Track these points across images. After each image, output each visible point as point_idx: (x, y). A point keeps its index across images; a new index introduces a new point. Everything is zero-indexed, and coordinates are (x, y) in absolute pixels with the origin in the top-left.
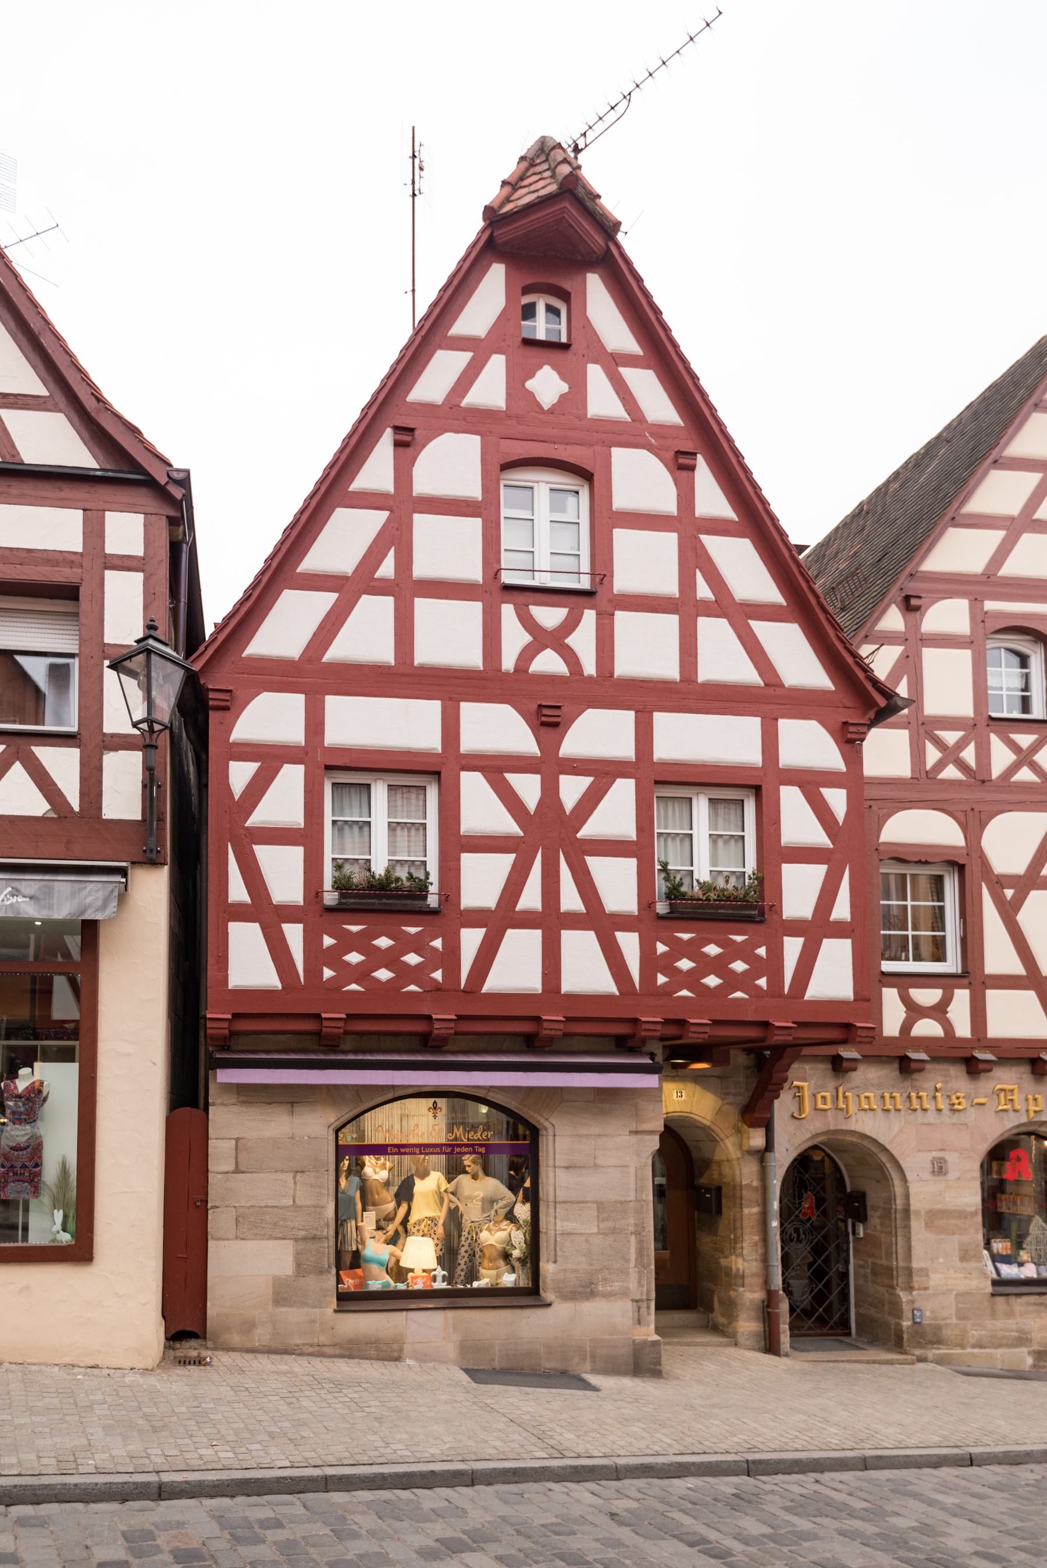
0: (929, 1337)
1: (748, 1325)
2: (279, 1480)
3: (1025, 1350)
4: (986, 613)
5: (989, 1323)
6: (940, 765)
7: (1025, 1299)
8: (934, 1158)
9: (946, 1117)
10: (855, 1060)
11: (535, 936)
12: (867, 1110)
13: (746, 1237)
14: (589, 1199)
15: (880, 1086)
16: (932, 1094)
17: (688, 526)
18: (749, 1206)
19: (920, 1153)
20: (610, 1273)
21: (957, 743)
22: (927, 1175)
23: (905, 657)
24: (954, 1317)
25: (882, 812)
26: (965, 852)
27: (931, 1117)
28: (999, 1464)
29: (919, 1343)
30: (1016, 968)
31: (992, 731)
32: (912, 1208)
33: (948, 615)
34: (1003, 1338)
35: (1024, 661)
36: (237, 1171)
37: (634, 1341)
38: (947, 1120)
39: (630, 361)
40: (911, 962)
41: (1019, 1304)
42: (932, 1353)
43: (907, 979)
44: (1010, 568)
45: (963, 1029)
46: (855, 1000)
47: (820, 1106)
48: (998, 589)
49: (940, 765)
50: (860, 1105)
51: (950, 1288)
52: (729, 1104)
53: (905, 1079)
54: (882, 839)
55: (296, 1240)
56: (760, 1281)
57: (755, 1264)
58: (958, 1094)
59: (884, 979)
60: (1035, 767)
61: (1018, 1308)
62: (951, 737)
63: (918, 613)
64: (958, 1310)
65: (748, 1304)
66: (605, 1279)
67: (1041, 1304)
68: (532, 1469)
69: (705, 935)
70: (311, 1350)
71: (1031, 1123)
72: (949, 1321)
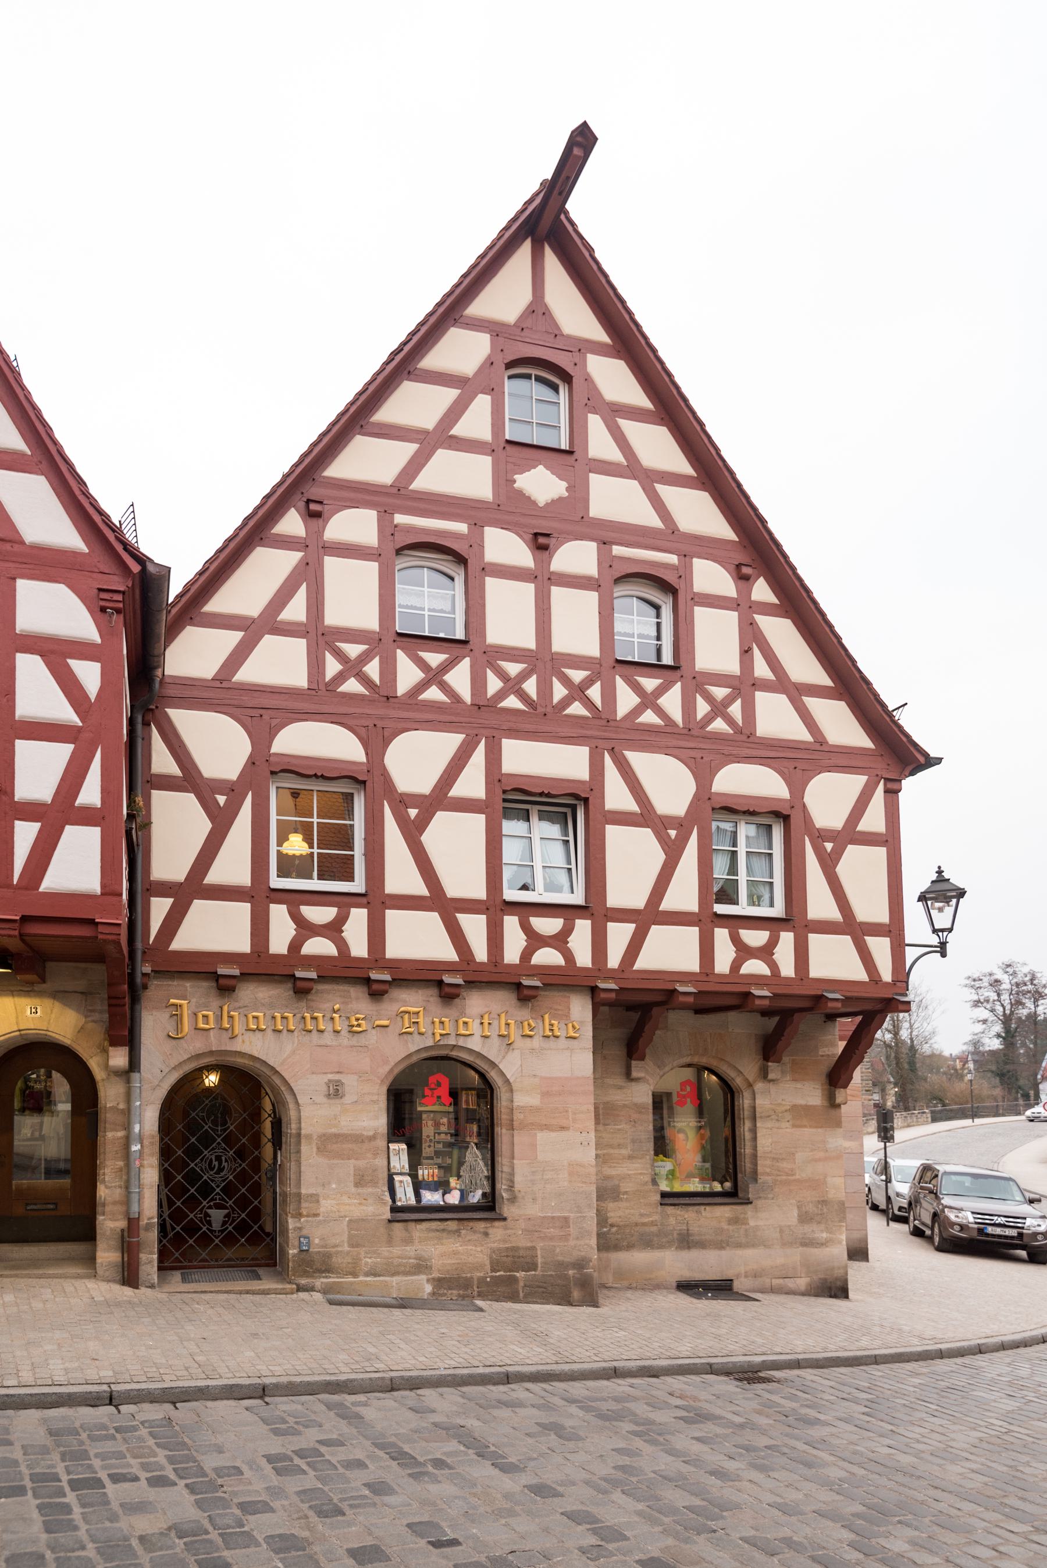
1: (107, 1255)
3: (424, 1277)
4: (396, 526)
5: (385, 1251)
7: (425, 1225)
9: (345, 1039)
10: (234, 977)
11: (613, 900)
12: (261, 1033)
13: (108, 1163)
15: (272, 1006)
16: (328, 1016)
17: (745, 608)
21: (360, 656)
22: (321, 1099)
23: (305, 563)
24: (346, 1245)
25: (274, 722)
26: (365, 768)
27: (328, 1038)
28: (151, 1402)
29: (305, 1272)
30: (418, 887)
31: (398, 648)
32: (303, 1132)
34: (400, 1265)
35: (657, 608)
38: (346, 1042)
41: (419, 1230)
42: (319, 1282)
43: (298, 896)
44: (422, 482)
45: (359, 948)
46: (102, 894)
47: (201, 1025)
48: (410, 503)
49: (340, 678)
50: (247, 1025)
51: (342, 1214)
52: (93, 1021)
53: (299, 1000)
54: (274, 749)
56: (122, 1208)
57: (118, 1191)
58: (358, 1016)
59: (273, 895)
60: (445, 687)
61: (418, 1234)
62: (353, 650)
63: (321, 521)
64: (351, 1237)
65: (108, 1233)
67: (443, 1230)
71: (436, 1046)
72: (339, 1249)
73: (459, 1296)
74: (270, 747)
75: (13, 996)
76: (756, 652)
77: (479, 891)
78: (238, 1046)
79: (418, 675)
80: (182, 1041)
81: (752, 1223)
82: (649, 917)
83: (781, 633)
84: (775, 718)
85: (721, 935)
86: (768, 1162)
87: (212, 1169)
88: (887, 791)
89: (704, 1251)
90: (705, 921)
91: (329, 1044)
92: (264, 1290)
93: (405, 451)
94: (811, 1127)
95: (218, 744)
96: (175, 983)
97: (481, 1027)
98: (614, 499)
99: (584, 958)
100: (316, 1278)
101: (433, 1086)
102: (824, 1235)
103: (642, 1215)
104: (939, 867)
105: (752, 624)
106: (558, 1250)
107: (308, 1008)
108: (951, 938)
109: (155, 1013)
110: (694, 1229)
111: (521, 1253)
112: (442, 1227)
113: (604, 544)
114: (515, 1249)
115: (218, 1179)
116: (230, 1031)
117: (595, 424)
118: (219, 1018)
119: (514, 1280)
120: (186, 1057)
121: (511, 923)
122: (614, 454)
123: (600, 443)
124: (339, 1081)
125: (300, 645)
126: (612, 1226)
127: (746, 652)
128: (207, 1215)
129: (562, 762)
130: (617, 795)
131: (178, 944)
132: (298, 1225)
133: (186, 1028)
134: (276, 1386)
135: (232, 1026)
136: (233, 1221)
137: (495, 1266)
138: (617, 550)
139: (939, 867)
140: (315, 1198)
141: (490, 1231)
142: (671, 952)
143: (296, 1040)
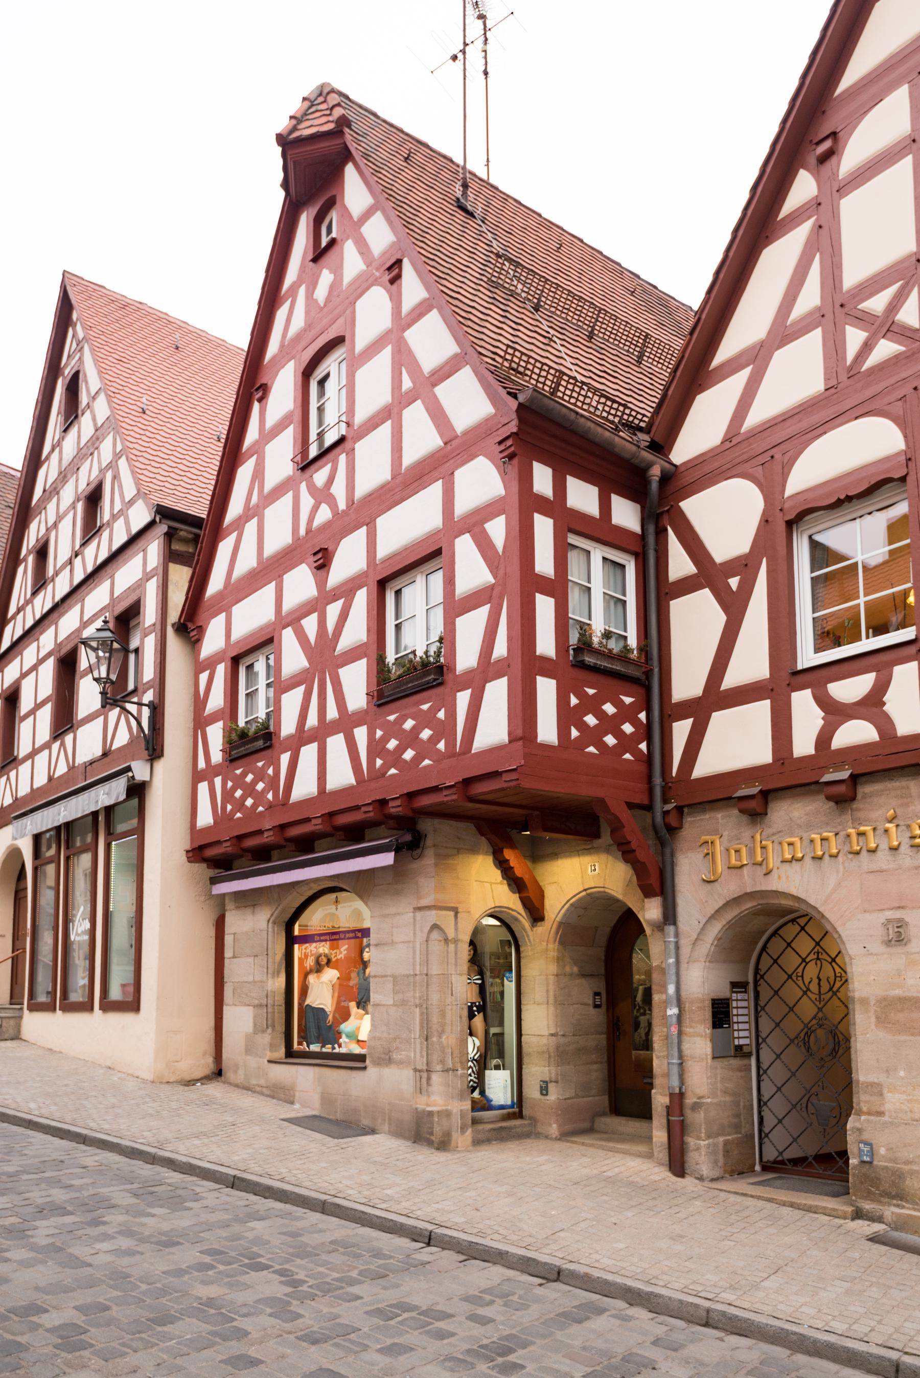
0: (885, 1186)
2: (830, 1346)
8: (889, 921)
14: (389, 973)
15: (809, 827)
19: (867, 915)
20: (401, 1043)
22: (877, 947)
27: (883, 859)
29: (869, 1192)
36: (234, 957)
37: (416, 1109)
40: (872, 640)
46: (510, 742)
53: (842, 812)
55: (254, 1006)
66: (397, 1048)
68: (113, 1143)
69: (403, 713)
70: (258, 1089)
75: (579, 855)
76: (57, 450)
78: (776, 883)
80: (716, 884)
91: (884, 867)
92: (810, 1207)
96: (707, 816)
100: (884, 1204)
107: (854, 820)
109: (690, 855)
116: (764, 866)
118: (752, 852)
120: (721, 903)
124: (900, 920)
131: (700, 770)
132: (858, 1125)
133: (719, 869)
134: (573, 1274)
135: (765, 859)
140: (877, 1089)
143: (841, 867)
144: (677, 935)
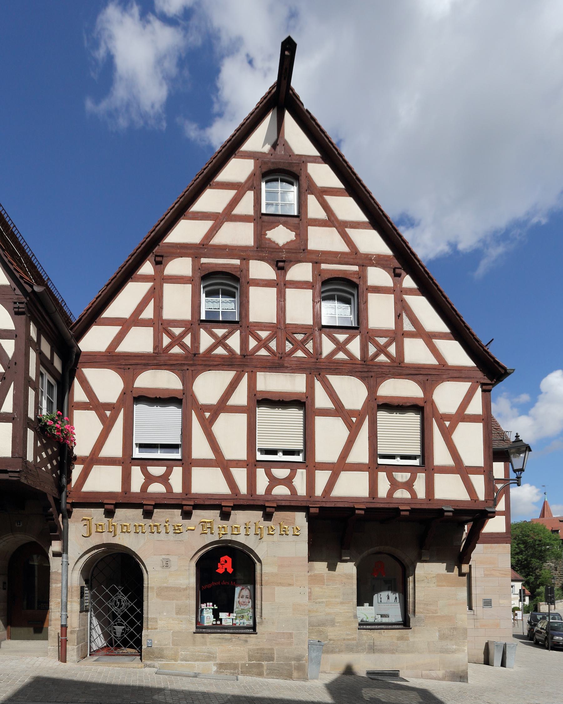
3: (212, 663)
6: (170, 346)
12: (129, 532)
17: (398, 293)
18: (56, 583)
23: (153, 289)
29: (150, 657)
30: (209, 454)
33: (181, 266)
39: (356, 225)
45: (177, 488)
49: (170, 346)
51: (169, 628)
63: (162, 266)
73: (231, 673)
74: (133, 384)
77: (243, 455)
79: (211, 341)
81: (411, 640)
82: (340, 466)
83: (421, 306)
84: (416, 352)
85: (382, 476)
86: (422, 606)
87: (116, 606)
88: (483, 391)
89: (383, 655)
90: (373, 468)
93: (206, 225)
94: (447, 586)
95: (106, 384)
97: (244, 528)
98: (322, 239)
99: (302, 490)
101: (223, 563)
102: (454, 647)
103: (347, 635)
104: (517, 434)
105: (403, 300)
106: (286, 650)
108: (523, 475)
110: (377, 643)
111: (265, 652)
112: (222, 637)
113: (316, 264)
114: (263, 649)
115: (119, 611)
117: (312, 200)
119: (262, 666)
121: (261, 473)
122: (321, 214)
123: (314, 209)
124: (167, 559)
125: (150, 331)
126: (330, 640)
127: (398, 317)
128: (114, 629)
129: (293, 383)
130: (322, 400)
132: (147, 633)
136: (127, 632)
137: (250, 658)
138: (324, 266)
139: (517, 434)
141: (248, 639)
142: (352, 487)
144: (67, 558)
